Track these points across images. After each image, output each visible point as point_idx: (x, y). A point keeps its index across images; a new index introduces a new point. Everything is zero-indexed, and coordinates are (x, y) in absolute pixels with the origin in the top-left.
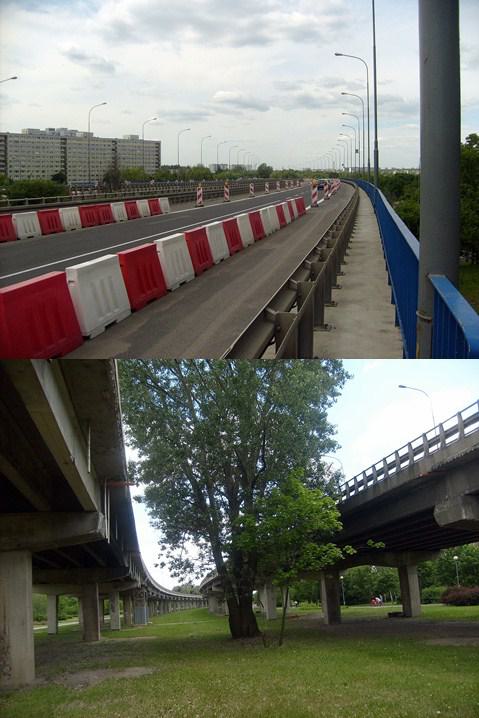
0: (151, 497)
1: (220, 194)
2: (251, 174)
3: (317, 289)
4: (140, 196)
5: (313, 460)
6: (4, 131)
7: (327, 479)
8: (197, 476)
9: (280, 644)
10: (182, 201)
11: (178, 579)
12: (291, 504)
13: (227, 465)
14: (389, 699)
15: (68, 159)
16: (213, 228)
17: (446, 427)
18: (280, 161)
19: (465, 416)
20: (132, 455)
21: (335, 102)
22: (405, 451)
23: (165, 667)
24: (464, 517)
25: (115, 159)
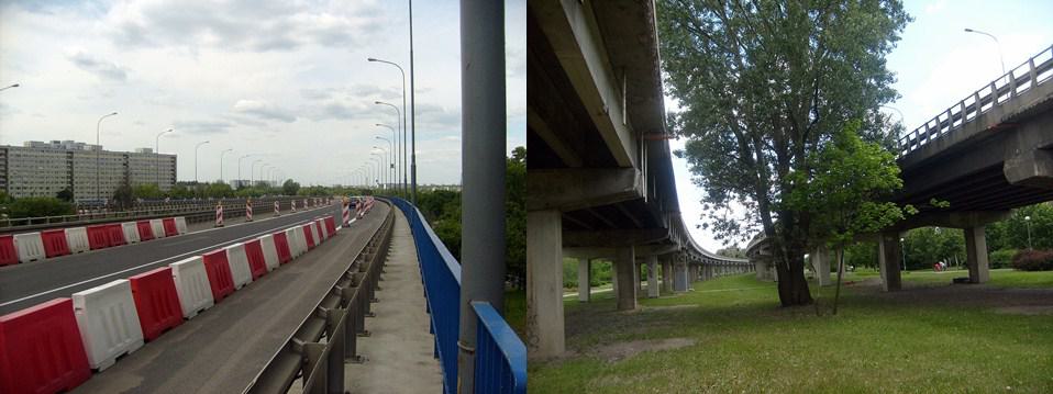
0: (693, 151)
1: (242, 213)
2: (275, 191)
3: (348, 317)
4: (154, 215)
5: (870, 111)
6: (4, 144)
7: (886, 131)
8: (744, 129)
9: (835, 313)
10: (200, 221)
11: (722, 241)
12: (846, 159)
13: (776, 119)
14: (954, 373)
15: (75, 175)
16: (234, 250)
17: (1017, 75)
18: (308, 177)
19: (1037, 63)
20: (672, 105)
21: (368, 112)
22: (972, 101)
23: (708, 338)
24: (1037, 173)
25: (127, 174)
